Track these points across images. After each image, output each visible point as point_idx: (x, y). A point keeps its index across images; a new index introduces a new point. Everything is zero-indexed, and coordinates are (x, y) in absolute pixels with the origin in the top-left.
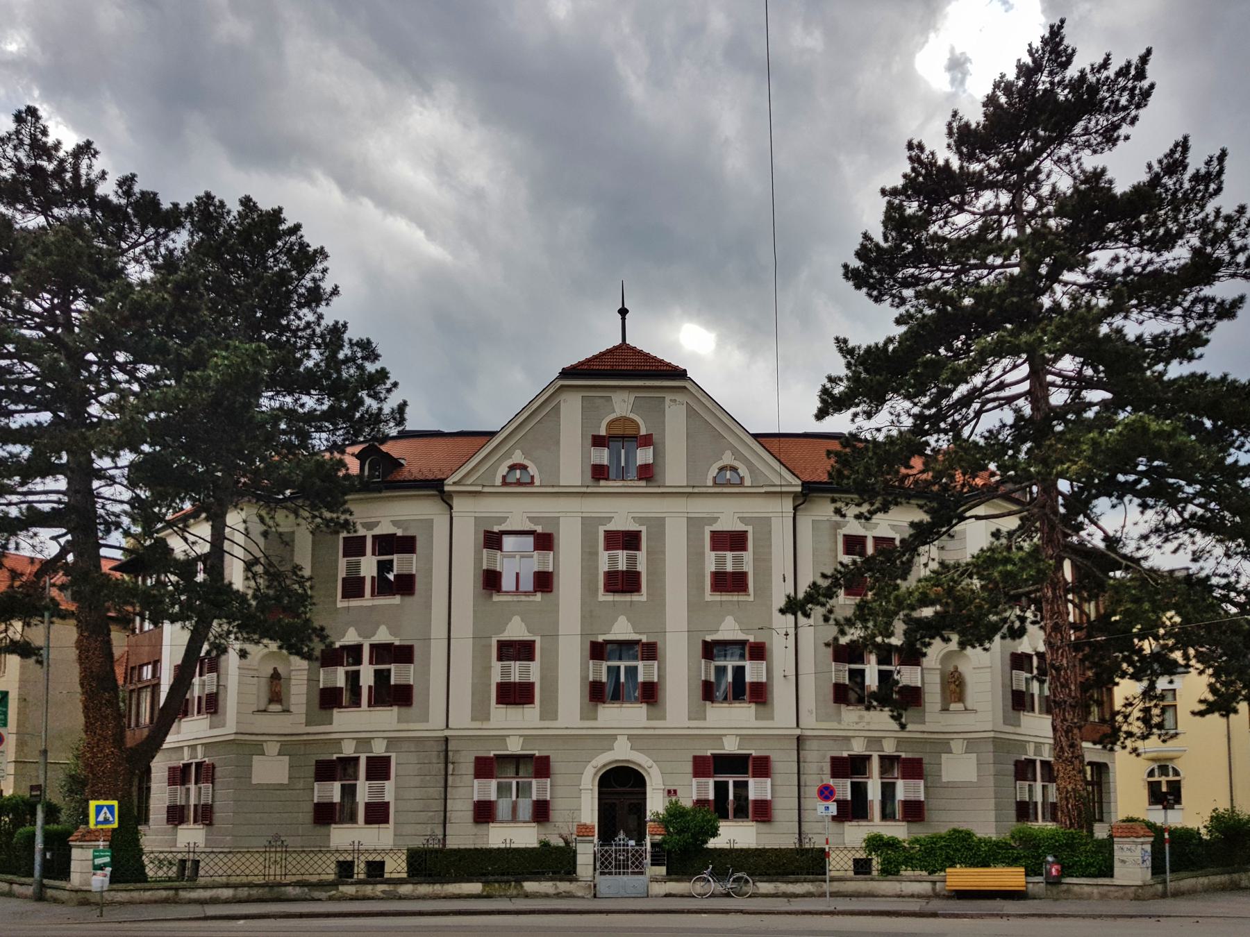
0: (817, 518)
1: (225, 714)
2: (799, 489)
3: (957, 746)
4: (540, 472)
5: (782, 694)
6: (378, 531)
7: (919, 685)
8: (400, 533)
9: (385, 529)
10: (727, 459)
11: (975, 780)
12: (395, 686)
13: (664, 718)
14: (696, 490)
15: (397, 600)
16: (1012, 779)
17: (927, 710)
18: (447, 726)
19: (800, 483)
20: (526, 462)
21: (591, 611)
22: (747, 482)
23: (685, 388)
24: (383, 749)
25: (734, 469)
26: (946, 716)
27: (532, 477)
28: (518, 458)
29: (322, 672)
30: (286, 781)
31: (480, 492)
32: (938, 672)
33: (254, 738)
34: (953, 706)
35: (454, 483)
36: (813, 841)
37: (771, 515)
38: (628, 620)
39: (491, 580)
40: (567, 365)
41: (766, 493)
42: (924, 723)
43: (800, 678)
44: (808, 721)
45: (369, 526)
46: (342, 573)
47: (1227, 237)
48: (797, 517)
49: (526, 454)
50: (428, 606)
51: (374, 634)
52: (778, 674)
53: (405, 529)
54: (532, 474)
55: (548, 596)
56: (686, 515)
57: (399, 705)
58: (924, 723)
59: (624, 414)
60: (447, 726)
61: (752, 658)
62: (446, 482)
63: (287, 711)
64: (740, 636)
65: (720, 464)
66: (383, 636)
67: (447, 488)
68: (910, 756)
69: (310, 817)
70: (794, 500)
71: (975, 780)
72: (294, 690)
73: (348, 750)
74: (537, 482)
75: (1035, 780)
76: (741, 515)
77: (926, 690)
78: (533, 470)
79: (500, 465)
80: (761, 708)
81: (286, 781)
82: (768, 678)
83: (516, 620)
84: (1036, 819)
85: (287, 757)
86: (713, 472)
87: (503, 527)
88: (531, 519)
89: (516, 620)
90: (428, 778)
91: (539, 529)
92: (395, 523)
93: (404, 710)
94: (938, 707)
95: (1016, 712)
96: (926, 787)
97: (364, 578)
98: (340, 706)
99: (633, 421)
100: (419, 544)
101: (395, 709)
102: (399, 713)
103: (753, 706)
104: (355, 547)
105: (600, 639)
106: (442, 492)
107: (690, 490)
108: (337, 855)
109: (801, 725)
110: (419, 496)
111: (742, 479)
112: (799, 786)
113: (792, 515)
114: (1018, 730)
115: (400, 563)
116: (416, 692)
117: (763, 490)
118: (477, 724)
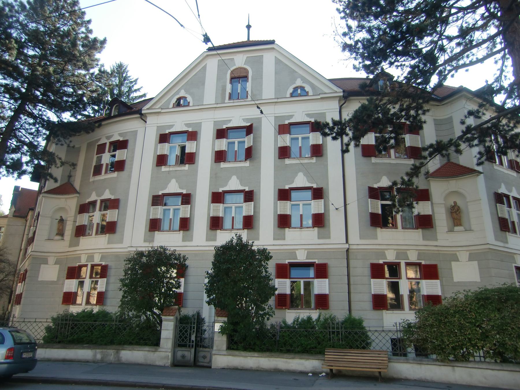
1: (488, 195)
4: (193, 100)
6: (113, 139)
7: (430, 213)
9: (116, 138)
14: (279, 100)
15: (115, 174)
17: (438, 231)
18: (233, 228)
19: (342, 91)
20: (186, 96)
22: (311, 93)
23: (273, 49)
25: (302, 88)
26: (451, 235)
27: (189, 103)
28: (182, 94)
29: (78, 217)
32: (443, 206)
33: (43, 254)
34: (456, 228)
35: (148, 109)
37: (325, 111)
38: (238, 178)
39: (161, 160)
41: (322, 98)
42: (436, 240)
43: (23, 234)
44: (355, 238)
45: (108, 138)
46: (94, 164)
47: (493, 39)
48: (343, 110)
49: (187, 91)
50: (130, 176)
52: (332, 208)
54: (189, 101)
56: (274, 115)
57: (109, 233)
58: (436, 240)
59: (240, 66)
60: (233, 228)
62: (143, 109)
65: (294, 86)
66: (107, 195)
67: (143, 112)
68: (428, 263)
70: (340, 101)
74: (191, 104)
76: (307, 113)
77: (436, 218)
78: (189, 99)
79: (172, 98)
80: (322, 230)
82: (496, 206)
83: (173, 181)
86: (291, 90)
89: (173, 181)
91: (190, 130)
92: (120, 135)
93: (112, 235)
94: (446, 229)
95: (503, 232)
96: (442, 285)
97: (103, 164)
99: (245, 69)
100: (130, 145)
101: (107, 235)
104: (101, 149)
106: (141, 114)
107: (276, 100)
109: (350, 242)
111: (307, 93)
112: (349, 284)
113: (338, 110)
114: (506, 245)
115: (120, 155)
117: (319, 97)
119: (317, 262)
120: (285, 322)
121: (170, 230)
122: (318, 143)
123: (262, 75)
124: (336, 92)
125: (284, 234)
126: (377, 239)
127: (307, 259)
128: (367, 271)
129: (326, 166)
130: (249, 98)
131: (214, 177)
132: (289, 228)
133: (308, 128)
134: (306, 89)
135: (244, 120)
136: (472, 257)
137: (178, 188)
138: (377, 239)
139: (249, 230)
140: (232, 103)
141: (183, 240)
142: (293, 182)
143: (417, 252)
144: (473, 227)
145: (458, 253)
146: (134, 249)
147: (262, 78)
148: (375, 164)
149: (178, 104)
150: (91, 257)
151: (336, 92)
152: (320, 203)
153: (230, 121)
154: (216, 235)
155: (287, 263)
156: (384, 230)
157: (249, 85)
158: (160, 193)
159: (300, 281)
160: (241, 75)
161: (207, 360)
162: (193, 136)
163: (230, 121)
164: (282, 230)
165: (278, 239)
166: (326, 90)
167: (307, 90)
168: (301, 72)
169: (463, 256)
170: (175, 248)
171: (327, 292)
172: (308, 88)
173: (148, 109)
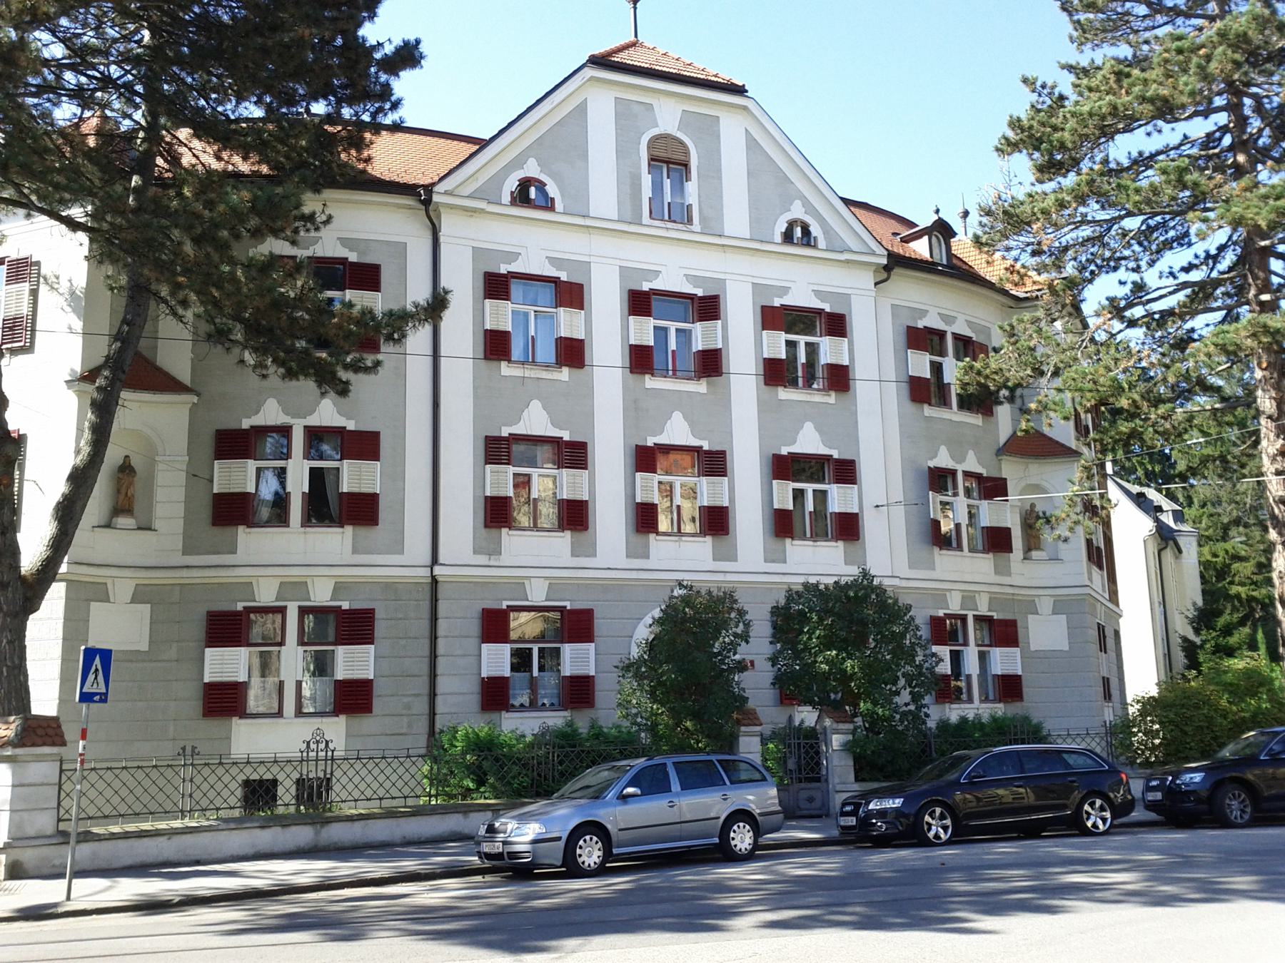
0: (897, 302)
2: (885, 261)
3: (1045, 605)
4: (562, 195)
5: (872, 527)
8: (353, 257)
10: (797, 212)
11: (1067, 648)
12: (351, 495)
13: (734, 558)
16: (474, 641)
20: (543, 178)
21: (635, 401)
23: (745, 108)
24: (329, 595)
25: (541, 186)
28: (532, 169)
30: (144, 646)
31: (482, 211)
35: (446, 193)
36: (331, 746)
37: (849, 291)
40: (596, 52)
41: (848, 261)
42: (1009, 574)
51: (312, 412)
53: (360, 254)
55: (844, 396)
58: (1009, 574)
61: (838, 481)
62: (436, 189)
63: (146, 527)
64: (822, 450)
67: (435, 198)
69: (196, 705)
71: (1067, 648)
72: (160, 494)
73: (266, 595)
75: (966, 644)
76: (816, 288)
78: (552, 190)
81: (144, 646)
84: (970, 700)
85: (1064, 617)
87: (516, 267)
88: (553, 261)
90: (403, 642)
93: (363, 531)
98: (251, 524)
99: (682, 143)
101: (349, 530)
102: (354, 537)
103: (841, 544)
105: (784, 451)
106: (427, 203)
108: (248, 770)
110: (387, 204)
115: (920, 364)
116: (383, 505)
118: (482, 559)
119: (568, 608)
120: (949, 719)
121: (535, 527)
122: (840, 362)
123: (719, 170)
124: (873, 253)
125: (784, 551)
126: (934, 569)
127: (277, 600)
128: (474, 627)
129: (854, 414)
130: (696, 225)
131: (634, 409)
132: (510, 528)
133: (547, 292)
134: (547, 188)
135: (817, 293)
136: (138, 597)
137: (549, 424)
138: (934, 569)
139: (577, 534)
140: (659, 228)
141: (574, 554)
142: (794, 442)
143: (1052, 599)
144: (157, 524)
145: (109, 582)
146: (801, 580)
147: (720, 178)
148: (929, 419)
149: (521, 196)
150: (299, 588)
151: (873, 253)
152: (849, 491)
153: (657, 273)
154: (647, 546)
155: (504, 607)
156: (944, 552)
157: (692, 187)
158: (505, 432)
159: (530, 650)
160: (674, 157)
161: (817, 804)
162: (708, 308)
163: (657, 273)
164: (494, 532)
165: (773, 561)
166: (853, 243)
167: (551, 195)
168: (801, 185)
169: (1045, 605)
170: (818, 578)
171: (592, 673)
172: (815, 230)
173: (446, 193)
